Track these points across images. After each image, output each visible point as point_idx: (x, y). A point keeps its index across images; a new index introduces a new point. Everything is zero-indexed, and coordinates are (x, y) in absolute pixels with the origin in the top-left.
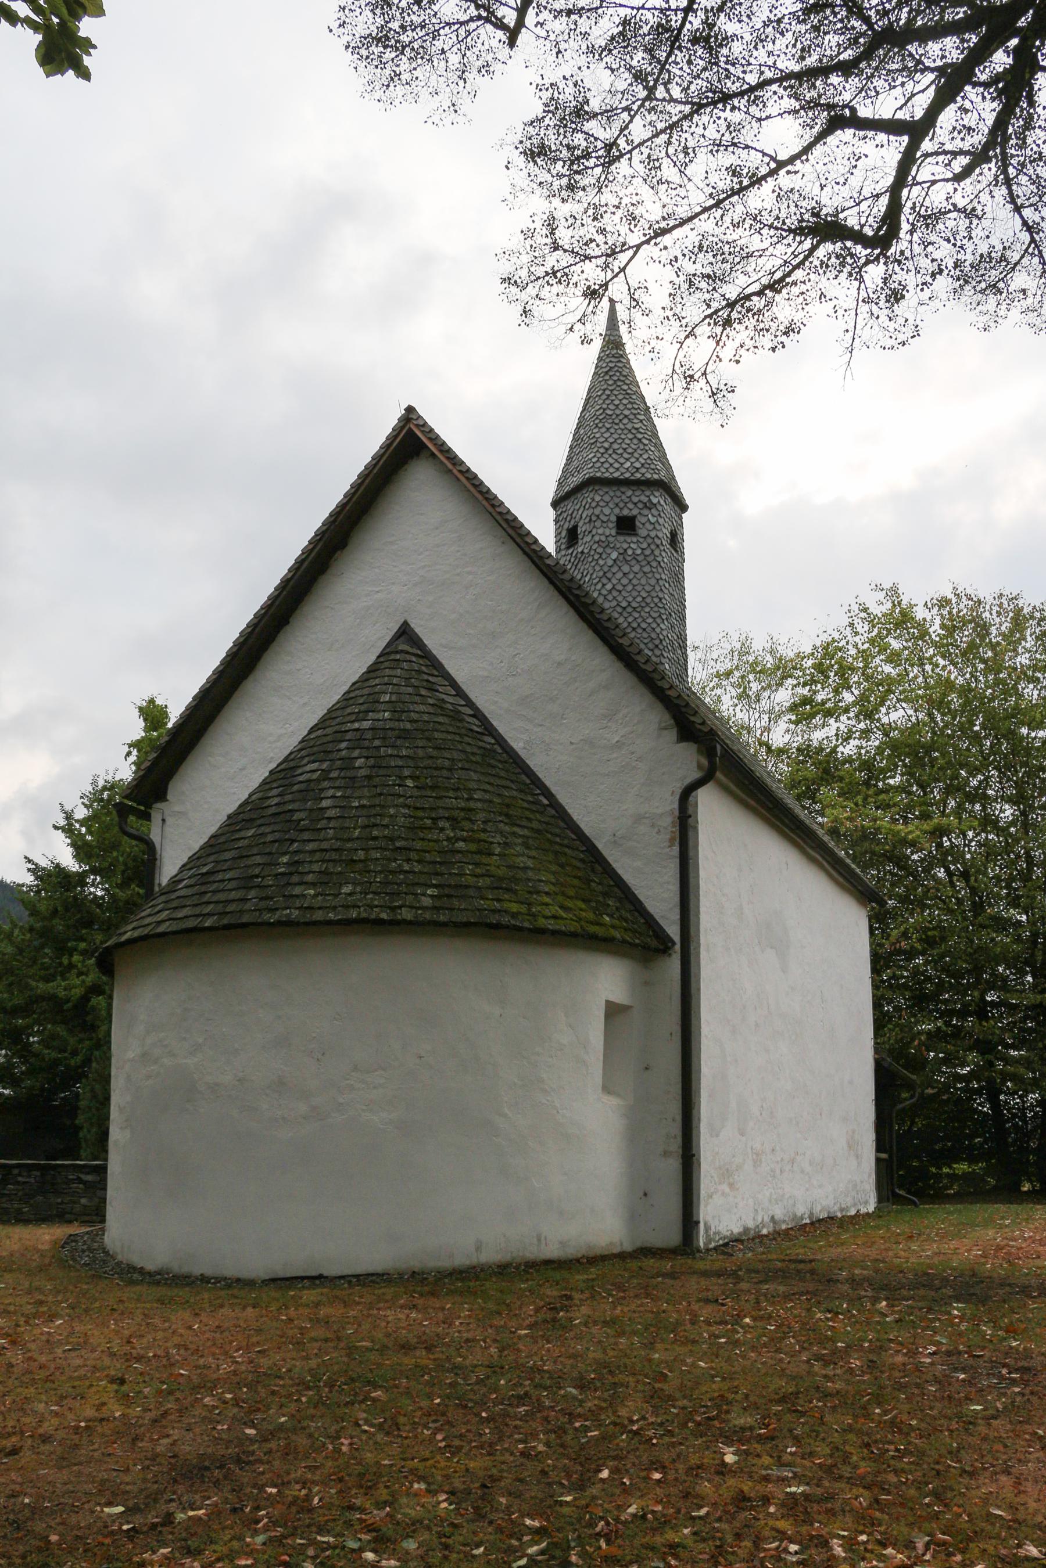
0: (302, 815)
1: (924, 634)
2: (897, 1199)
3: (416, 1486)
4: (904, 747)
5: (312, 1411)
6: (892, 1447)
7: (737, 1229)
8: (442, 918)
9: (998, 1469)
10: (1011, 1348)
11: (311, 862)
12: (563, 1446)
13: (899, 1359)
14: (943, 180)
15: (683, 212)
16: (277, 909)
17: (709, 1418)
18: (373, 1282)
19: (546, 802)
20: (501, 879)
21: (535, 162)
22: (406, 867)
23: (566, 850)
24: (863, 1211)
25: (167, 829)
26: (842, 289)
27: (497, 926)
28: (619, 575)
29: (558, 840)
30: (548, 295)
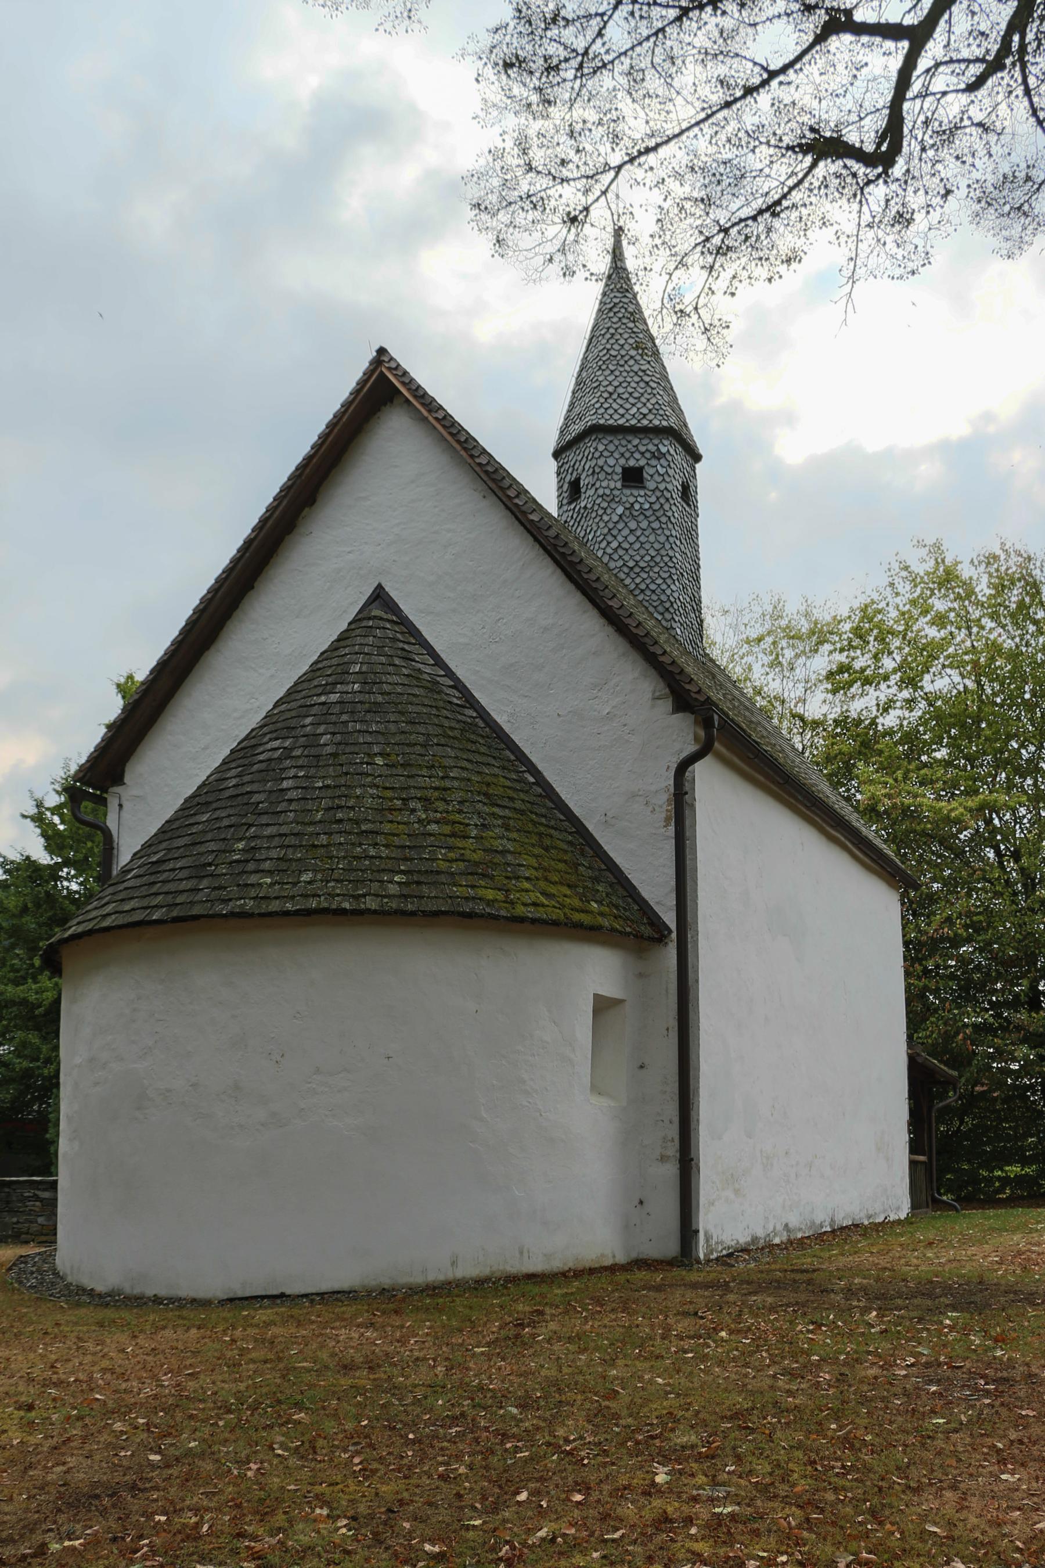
0: (261, 797)
1: (970, 593)
2: (937, 1204)
3: (318, 1511)
4: (955, 720)
5: (227, 1435)
6: (839, 1464)
7: (743, 1239)
8: (410, 907)
9: (945, 1485)
10: (995, 1358)
11: (268, 848)
12: (487, 1468)
13: (872, 1372)
14: (957, 91)
15: (672, 129)
16: (230, 900)
17: (652, 1437)
18: (337, 1300)
19: (532, 780)
20: (477, 864)
21: (509, 76)
22: (372, 852)
23: (552, 832)
24: (893, 1217)
25: (124, 814)
26: (843, 213)
27: (470, 915)
28: (626, 532)
29: (543, 820)
30: (523, 222)
